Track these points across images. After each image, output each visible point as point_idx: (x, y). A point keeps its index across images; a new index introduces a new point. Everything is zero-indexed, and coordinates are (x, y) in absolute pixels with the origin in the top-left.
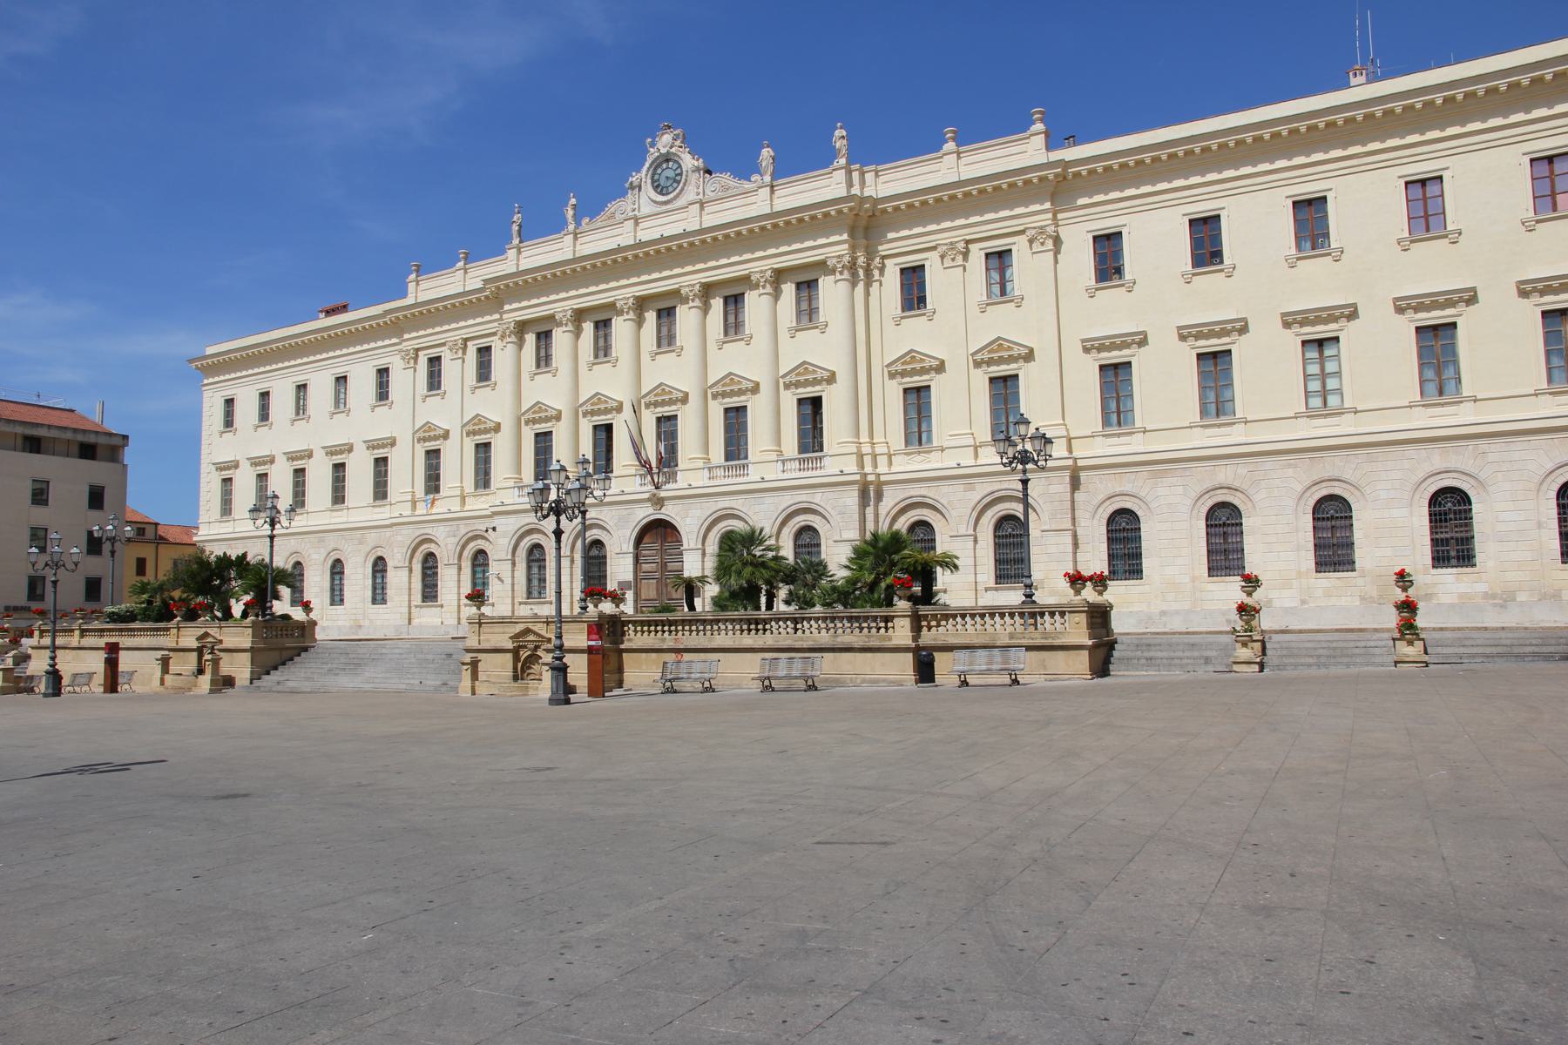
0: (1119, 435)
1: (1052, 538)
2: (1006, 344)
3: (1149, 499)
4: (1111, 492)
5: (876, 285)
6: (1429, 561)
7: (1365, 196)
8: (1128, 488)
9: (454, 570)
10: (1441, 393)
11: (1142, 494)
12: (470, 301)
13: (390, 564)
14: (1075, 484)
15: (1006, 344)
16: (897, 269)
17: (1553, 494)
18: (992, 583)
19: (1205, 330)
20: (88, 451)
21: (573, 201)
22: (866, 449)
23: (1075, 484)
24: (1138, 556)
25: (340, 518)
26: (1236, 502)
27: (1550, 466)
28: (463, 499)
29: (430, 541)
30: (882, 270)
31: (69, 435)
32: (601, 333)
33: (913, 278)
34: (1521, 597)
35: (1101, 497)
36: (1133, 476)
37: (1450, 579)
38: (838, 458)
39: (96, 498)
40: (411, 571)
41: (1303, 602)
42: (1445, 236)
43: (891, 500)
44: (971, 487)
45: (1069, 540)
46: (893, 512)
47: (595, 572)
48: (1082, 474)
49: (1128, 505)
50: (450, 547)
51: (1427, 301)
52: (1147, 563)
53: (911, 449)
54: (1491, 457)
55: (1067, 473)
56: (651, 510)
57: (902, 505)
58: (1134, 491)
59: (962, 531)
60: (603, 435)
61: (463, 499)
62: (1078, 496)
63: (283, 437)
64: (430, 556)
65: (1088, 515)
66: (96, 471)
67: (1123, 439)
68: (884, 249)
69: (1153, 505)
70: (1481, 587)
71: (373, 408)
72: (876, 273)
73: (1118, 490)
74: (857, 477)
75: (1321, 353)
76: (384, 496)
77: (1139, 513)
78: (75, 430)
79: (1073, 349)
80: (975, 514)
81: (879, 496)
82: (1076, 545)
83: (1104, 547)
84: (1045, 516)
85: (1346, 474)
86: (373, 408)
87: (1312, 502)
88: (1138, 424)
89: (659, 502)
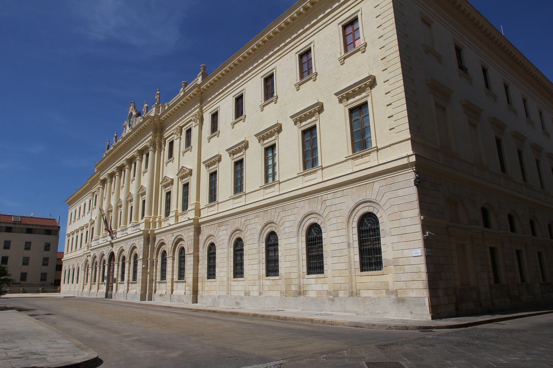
7: (285, 66)
9: (83, 272)
12: (181, 104)
14: (198, 231)
19: (350, 91)
25: (241, 202)
27: (352, 205)
31: (39, 227)
34: (341, 294)
37: (313, 281)
39: (47, 247)
41: (260, 294)
42: (359, 50)
47: (182, 267)
54: (328, 203)
55: (193, 226)
63: (230, 134)
67: (366, 159)
70: (326, 287)
71: (298, 86)
76: (314, 162)
78: (42, 226)
86: (298, 86)
89: (112, 244)
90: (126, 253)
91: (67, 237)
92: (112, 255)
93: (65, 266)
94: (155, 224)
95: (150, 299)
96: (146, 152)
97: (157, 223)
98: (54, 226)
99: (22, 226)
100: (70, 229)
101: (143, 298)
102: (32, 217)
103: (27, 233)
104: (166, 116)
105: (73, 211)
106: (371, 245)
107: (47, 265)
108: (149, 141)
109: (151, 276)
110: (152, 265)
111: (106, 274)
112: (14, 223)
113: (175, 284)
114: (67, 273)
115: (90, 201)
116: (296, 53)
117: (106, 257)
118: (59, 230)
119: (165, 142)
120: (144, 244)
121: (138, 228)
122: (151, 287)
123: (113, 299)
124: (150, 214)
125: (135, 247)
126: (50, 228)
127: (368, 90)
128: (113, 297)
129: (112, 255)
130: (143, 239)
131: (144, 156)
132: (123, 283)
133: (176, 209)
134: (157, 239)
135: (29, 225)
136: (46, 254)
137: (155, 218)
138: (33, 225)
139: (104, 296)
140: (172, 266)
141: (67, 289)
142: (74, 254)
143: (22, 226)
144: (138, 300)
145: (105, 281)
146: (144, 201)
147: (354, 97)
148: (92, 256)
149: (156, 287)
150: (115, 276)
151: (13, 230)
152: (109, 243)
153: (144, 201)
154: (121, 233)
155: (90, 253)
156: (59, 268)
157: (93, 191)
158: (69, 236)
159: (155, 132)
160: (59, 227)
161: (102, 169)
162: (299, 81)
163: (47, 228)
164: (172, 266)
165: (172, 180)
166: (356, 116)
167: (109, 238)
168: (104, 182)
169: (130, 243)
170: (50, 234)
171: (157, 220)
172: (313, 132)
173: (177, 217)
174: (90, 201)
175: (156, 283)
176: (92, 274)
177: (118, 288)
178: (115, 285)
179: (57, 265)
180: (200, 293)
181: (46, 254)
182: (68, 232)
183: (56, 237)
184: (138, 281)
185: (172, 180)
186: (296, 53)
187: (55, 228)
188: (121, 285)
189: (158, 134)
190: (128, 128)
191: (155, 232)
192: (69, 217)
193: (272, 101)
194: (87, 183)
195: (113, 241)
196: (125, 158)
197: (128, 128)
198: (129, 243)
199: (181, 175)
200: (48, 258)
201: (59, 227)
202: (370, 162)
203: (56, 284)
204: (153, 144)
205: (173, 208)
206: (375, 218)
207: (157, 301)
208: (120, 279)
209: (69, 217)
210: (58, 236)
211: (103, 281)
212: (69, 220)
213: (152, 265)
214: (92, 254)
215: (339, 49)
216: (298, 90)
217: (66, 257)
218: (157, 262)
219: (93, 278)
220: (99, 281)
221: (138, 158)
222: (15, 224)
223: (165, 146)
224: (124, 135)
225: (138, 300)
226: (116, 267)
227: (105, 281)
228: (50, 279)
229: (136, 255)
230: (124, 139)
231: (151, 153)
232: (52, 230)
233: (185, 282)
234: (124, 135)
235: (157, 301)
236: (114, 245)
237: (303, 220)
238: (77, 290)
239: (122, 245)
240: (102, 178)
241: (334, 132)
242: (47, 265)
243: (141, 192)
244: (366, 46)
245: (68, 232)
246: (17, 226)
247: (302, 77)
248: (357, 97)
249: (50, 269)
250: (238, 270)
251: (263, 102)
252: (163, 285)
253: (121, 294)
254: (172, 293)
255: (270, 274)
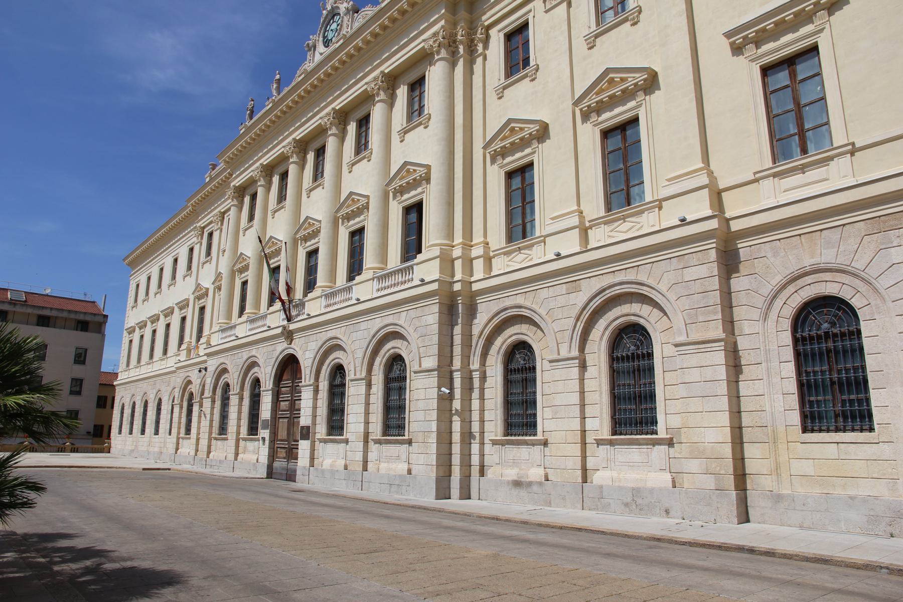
0: (803, 169)
1: (558, 374)
2: (617, 76)
3: (872, 272)
4: (793, 267)
5: (479, 60)
6: (795, 418)
8: (827, 257)
9: (363, 389)
10: (524, 237)
11: (859, 265)
13: (412, 365)
14: (729, 262)
15: (617, 76)
16: (502, 35)
17: (787, 324)
18: (606, 434)
20: (83, 326)
21: (278, 77)
22: (457, 252)
23: (729, 262)
24: (861, 384)
26: (845, 294)
28: (584, 232)
29: (339, 347)
30: (486, 41)
31: (65, 315)
32: (417, 93)
33: (517, 38)
35: (777, 279)
36: (835, 235)
38: (672, 193)
39: (80, 358)
40: (369, 385)
43: (486, 312)
44: (574, 286)
45: (719, 357)
46: (487, 331)
48: (742, 245)
49: (831, 289)
50: (360, 354)
51: (769, 24)
52: (878, 399)
53: (617, 213)
55: (712, 244)
56: (285, 345)
57: (496, 321)
58: (842, 260)
59: (564, 353)
60: (413, 217)
61: (584, 232)
62: (738, 283)
64: (397, 360)
65: (756, 314)
66: (82, 339)
67: (813, 174)
68: (487, 18)
69: (883, 283)
72: (480, 48)
73: (808, 262)
74: (714, 224)
75: (793, 75)
77: (856, 302)
78: (70, 312)
79: (715, 48)
80: (580, 326)
81: (472, 311)
82: (735, 366)
83: (790, 369)
84: (678, 320)
85: (849, 261)
87: (789, 311)
88: (839, 139)
89: (289, 335)
90: (233, 378)
91: (125, 333)
92: (289, 366)
93: (122, 397)
94: (469, 263)
95: (466, 494)
96: (251, 191)
97: (458, 264)
98: (95, 314)
99: (29, 310)
100: (132, 318)
101: (443, 492)
102: (47, 295)
103: (38, 325)
104: (218, 183)
105: (143, 279)
106: (522, 393)
107: (79, 393)
108: (290, 143)
109: (467, 423)
110: (468, 387)
111: (265, 412)
112: (13, 302)
113: (373, 447)
114: (127, 412)
115: (191, 250)
116: (499, 31)
117: (266, 374)
118: (105, 322)
119: (488, 37)
120: (441, 324)
121: (232, 332)
122: (466, 456)
123: (298, 485)
124: (450, 233)
125: (225, 371)
126: (88, 318)
127: (641, 96)
128: (299, 477)
129: (289, 366)
130: (436, 308)
131: (247, 199)
132: (189, 438)
133: (482, 239)
134: (480, 308)
135: (43, 308)
136: (79, 371)
137: (468, 245)
138: (51, 309)
139: (263, 472)
140: (362, 405)
141: (127, 448)
142: (145, 370)
143: (29, 310)
144: (429, 499)
145: (265, 433)
146: (245, 283)
147: (513, 155)
148: (211, 369)
149: (482, 455)
150: (305, 420)
151: (10, 317)
152: (279, 330)
153: (245, 283)
154: (221, 335)
155: (205, 361)
156: (105, 401)
157: (201, 224)
158: (131, 331)
159: (453, 9)
160: (106, 316)
161: (236, 163)
162: (594, 27)
163: (81, 317)
164: (362, 405)
165: (207, 289)
166: (517, 182)
167: (276, 319)
168: (247, 191)
169: (245, 354)
170: (86, 331)
171: (477, 251)
172: (527, 175)
173: (189, 351)
174: (191, 250)
175: (482, 444)
176: (212, 414)
177: (213, 448)
178: (304, 446)
179: (99, 398)
180: (730, 481)
181: (79, 371)
182: (131, 320)
183: (100, 335)
184: (229, 436)
185: (207, 289)
186: (499, 31)
187: (101, 319)
188: (219, 442)
189: (463, 14)
190: (321, 48)
191: (475, 287)
192: (132, 293)
193: (526, 76)
194: (186, 207)
195: (292, 327)
196: (258, 164)
197: (321, 48)
198: (363, 326)
199: (197, 294)
200: (81, 380)
201: (106, 316)
202: (642, 226)
203: (99, 436)
204: (451, 43)
205: (187, 339)
206: (643, 335)
207: (492, 499)
208: (321, 430)
209: (132, 293)
210: (104, 335)
211: (253, 429)
212: (131, 300)
213: (468, 387)
214: (213, 364)
215: (497, 74)
216: (500, 98)
217: (122, 377)
218: (483, 378)
219: (216, 424)
220: (238, 433)
221: (262, 182)
222: (15, 304)
223: (486, 47)
224: (308, 66)
225: (429, 499)
226: (306, 396)
227: (265, 433)
228: (86, 423)
229: (227, 386)
230: (309, 75)
231: (292, 170)
232: (90, 323)
233: (347, 442)
234: (308, 66)
235: (492, 499)
236: (296, 336)
237: (784, 287)
238: (156, 449)
239: (254, 353)
240: (237, 182)
241: (569, 176)
242: (79, 393)
243: (238, 266)
244: (640, 12)
245: (131, 320)
246: (18, 309)
247: (508, 75)
248: (518, 155)
249: (85, 403)
250: (143, 432)
251: (503, 80)
252: (251, 445)
253: (333, 472)
254: (236, 459)
255: (514, 431)
